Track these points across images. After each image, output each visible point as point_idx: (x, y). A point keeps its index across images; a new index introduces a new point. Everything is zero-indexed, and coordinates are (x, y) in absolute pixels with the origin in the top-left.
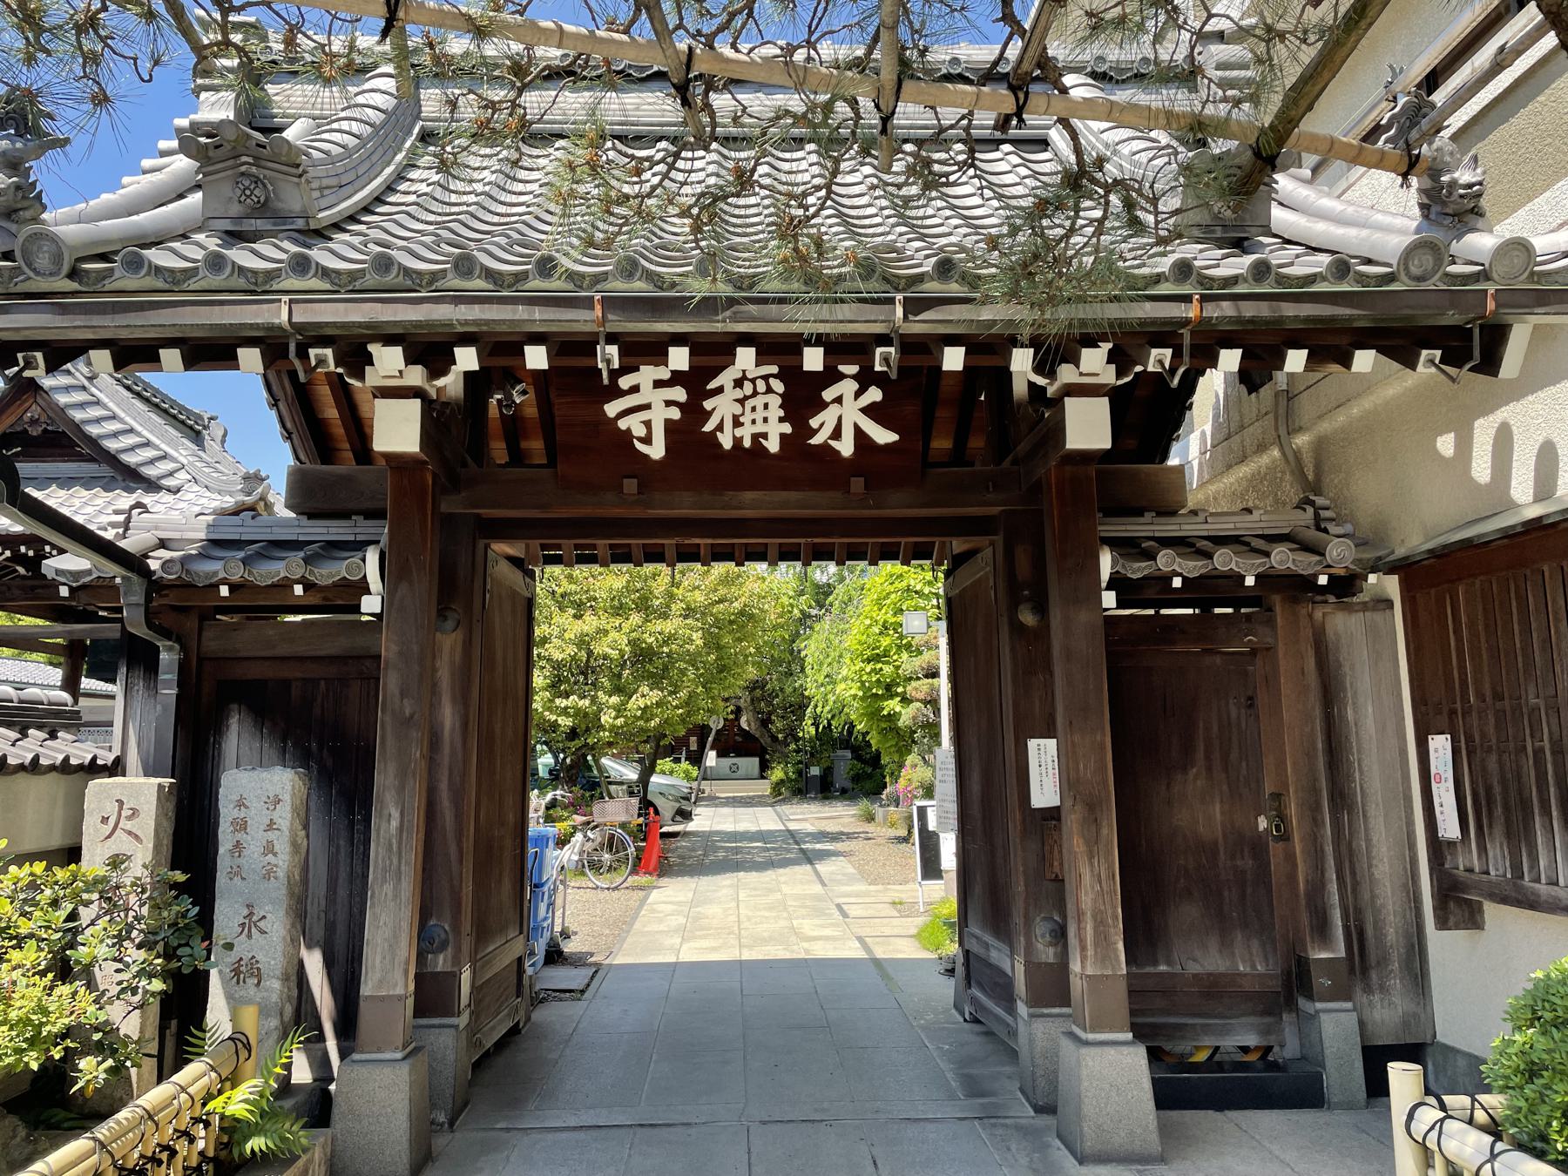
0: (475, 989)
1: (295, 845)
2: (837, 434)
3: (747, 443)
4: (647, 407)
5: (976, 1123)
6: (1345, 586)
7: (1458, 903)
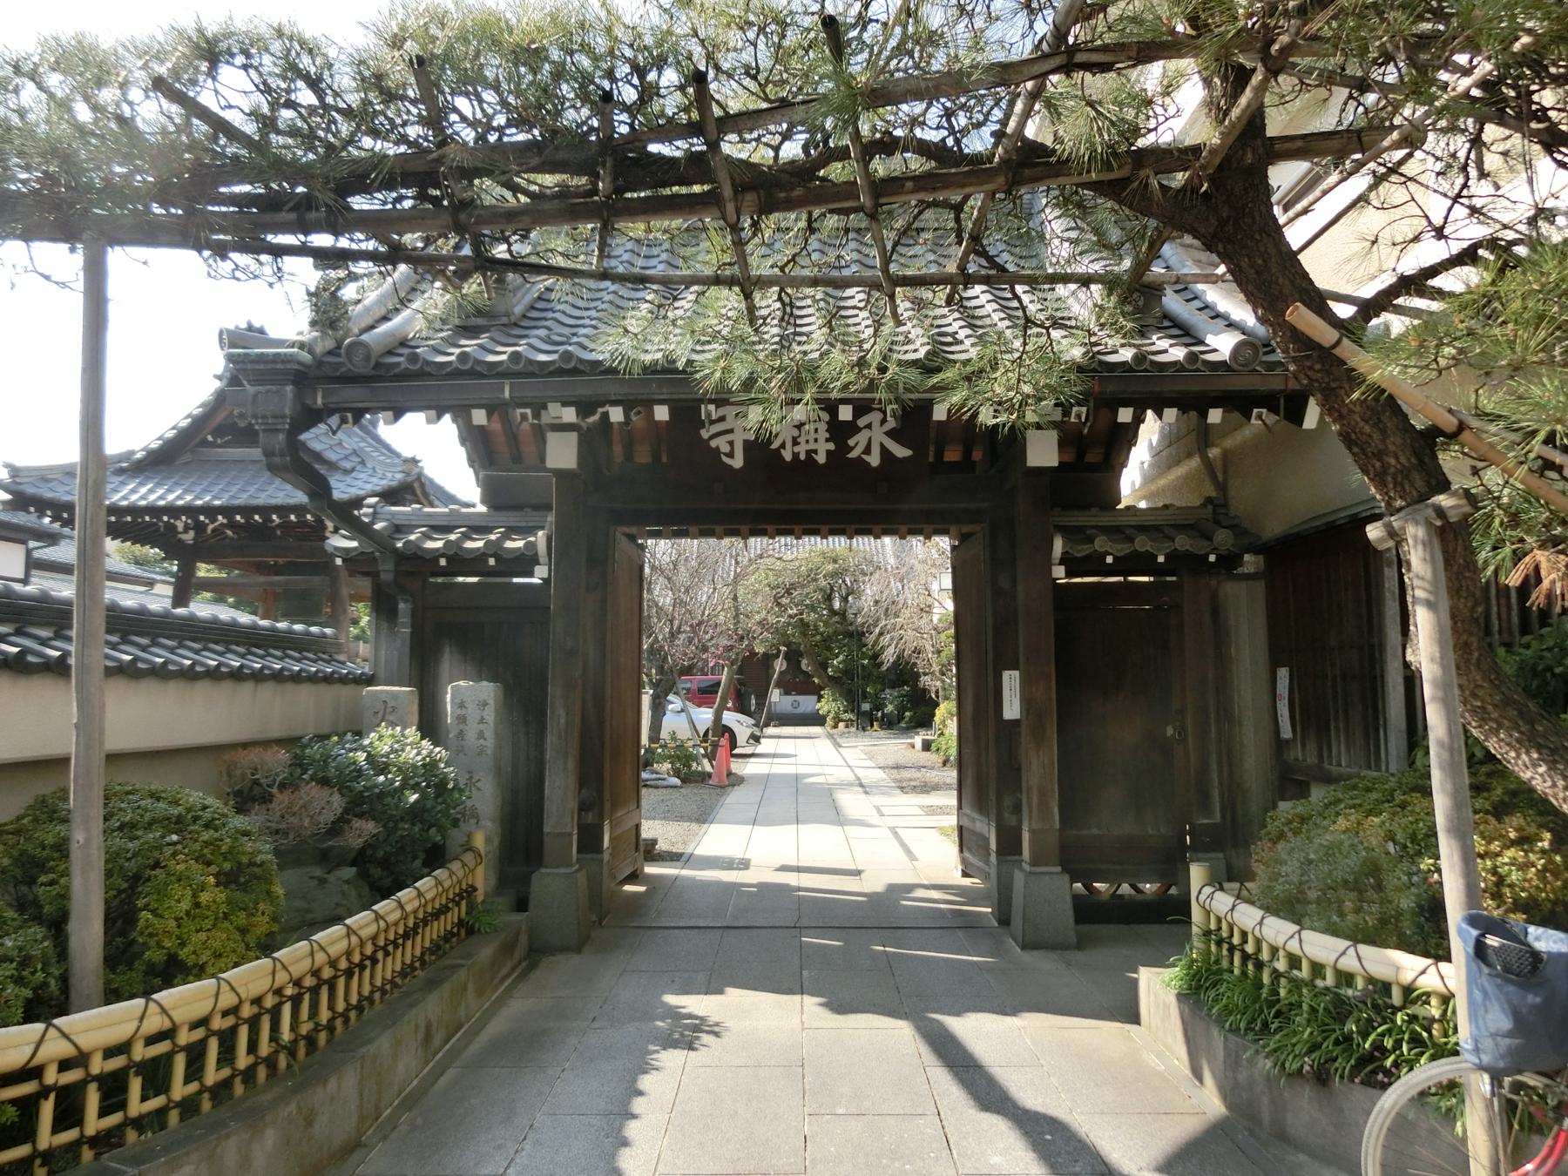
0: (611, 839)
1: (496, 733)
2: (868, 450)
3: (802, 457)
4: (731, 431)
5: (960, 933)
6: (1229, 562)
7: (1291, 783)
